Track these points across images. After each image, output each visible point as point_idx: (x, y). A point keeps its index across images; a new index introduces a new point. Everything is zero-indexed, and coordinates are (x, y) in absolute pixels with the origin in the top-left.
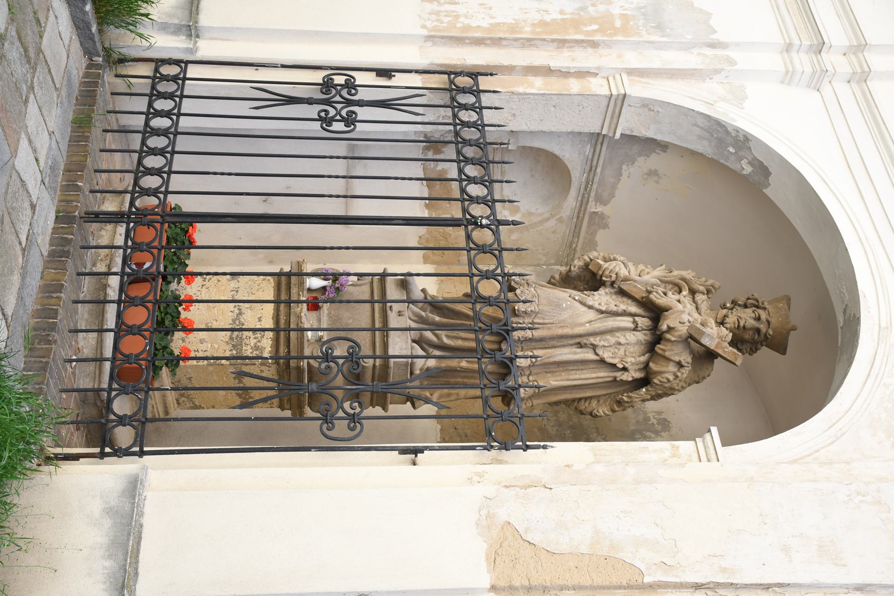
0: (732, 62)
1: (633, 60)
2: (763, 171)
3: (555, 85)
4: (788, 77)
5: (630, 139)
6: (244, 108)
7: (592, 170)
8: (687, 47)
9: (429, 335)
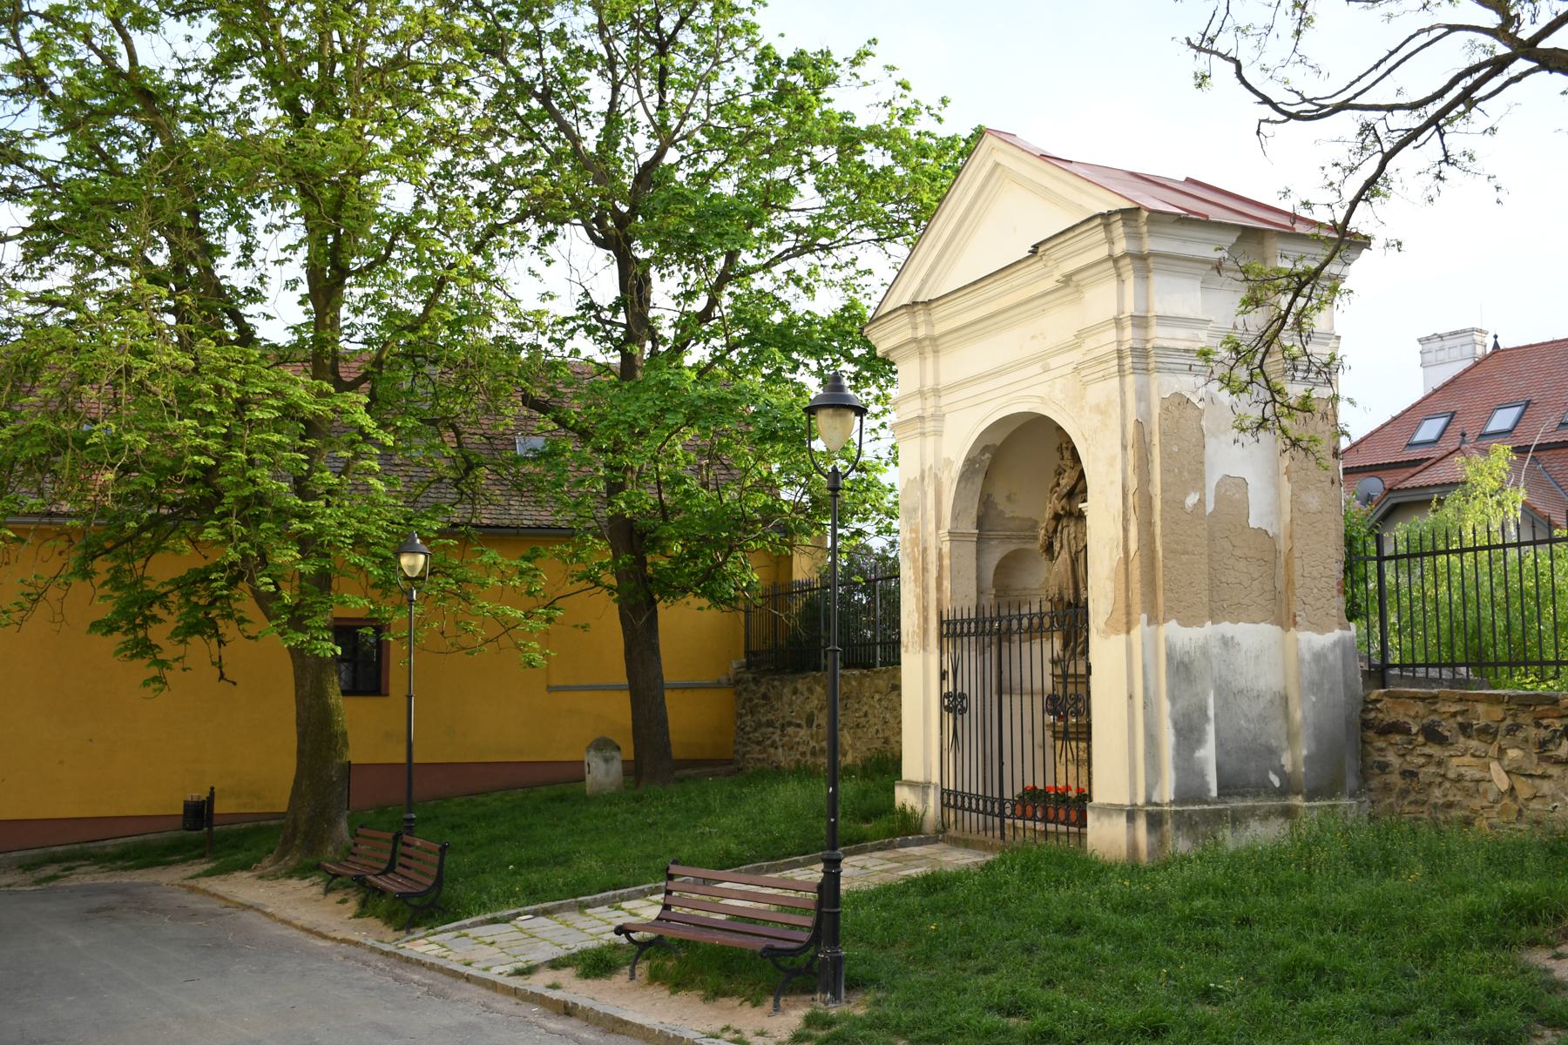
0: (931, 468)
1: (932, 526)
2: (985, 449)
3: (946, 573)
4: (938, 433)
5: (980, 524)
6: (959, 755)
7: (1009, 537)
8: (924, 494)
9: (1079, 649)
